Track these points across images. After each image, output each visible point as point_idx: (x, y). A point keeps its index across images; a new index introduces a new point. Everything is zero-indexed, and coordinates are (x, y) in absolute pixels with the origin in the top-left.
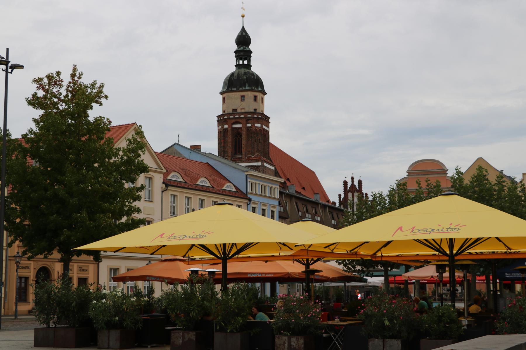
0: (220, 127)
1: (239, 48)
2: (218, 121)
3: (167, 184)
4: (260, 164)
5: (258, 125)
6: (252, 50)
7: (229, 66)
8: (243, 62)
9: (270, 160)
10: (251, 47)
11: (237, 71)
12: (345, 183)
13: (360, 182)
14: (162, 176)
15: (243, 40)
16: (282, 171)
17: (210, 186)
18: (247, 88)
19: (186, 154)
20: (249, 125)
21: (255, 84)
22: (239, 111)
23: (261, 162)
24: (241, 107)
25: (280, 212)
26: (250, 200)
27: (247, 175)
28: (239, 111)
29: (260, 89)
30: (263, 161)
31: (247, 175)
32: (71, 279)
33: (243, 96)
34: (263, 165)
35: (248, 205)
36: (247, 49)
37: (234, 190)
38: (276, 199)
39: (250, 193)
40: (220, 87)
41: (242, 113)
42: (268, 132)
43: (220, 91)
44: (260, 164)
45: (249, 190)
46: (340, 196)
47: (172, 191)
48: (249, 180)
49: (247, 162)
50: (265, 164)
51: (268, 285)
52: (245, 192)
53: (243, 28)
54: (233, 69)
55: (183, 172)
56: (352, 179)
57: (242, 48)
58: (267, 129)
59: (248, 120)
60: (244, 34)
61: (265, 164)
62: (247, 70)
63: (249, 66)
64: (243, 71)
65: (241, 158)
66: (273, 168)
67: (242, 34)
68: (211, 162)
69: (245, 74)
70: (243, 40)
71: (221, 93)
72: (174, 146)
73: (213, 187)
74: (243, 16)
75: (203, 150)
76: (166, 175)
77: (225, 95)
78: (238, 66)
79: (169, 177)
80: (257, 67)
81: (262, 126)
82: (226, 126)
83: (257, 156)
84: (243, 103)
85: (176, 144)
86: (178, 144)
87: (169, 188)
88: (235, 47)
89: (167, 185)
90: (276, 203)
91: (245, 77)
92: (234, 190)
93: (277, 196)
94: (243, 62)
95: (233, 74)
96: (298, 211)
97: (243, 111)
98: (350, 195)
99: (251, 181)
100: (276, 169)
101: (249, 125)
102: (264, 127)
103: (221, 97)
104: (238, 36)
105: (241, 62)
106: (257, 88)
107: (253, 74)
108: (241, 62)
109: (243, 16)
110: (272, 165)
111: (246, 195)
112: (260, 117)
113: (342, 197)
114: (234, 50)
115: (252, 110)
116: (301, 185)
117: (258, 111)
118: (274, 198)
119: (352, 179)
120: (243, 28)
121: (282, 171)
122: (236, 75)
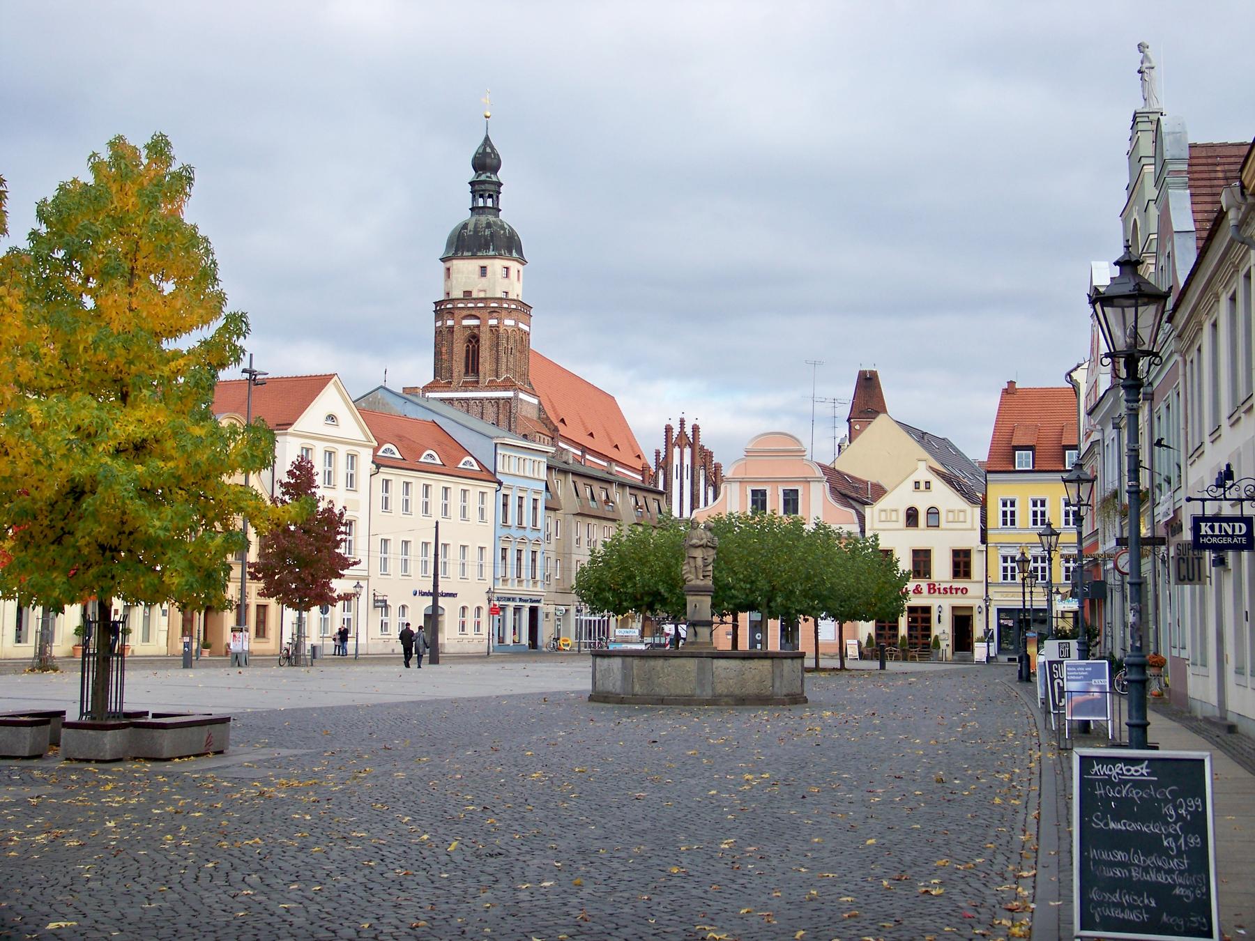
3: (379, 464)
4: (510, 394)
5: (509, 322)
7: (458, 208)
8: (485, 202)
11: (474, 219)
12: (668, 429)
13: (695, 429)
14: (371, 451)
15: (486, 162)
16: (553, 407)
18: (492, 253)
19: (399, 407)
21: (509, 245)
22: (474, 295)
24: (480, 287)
25: (546, 500)
26: (500, 484)
28: (474, 295)
29: (514, 254)
32: (247, 606)
33: (483, 270)
34: (516, 397)
36: (494, 179)
41: (481, 300)
43: (441, 256)
44: (510, 394)
45: (499, 468)
46: (658, 453)
47: (385, 473)
48: (499, 451)
51: (744, 645)
53: (487, 139)
55: (399, 440)
56: (682, 422)
58: (526, 328)
61: (522, 396)
62: (492, 218)
65: (477, 382)
66: (535, 401)
68: (439, 420)
69: (489, 225)
70: (486, 162)
71: (443, 260)
76: (376, 450)
77: (448, 264)
79: (380, 453)
80: (513, 210)
81: (516, 324)
83: (507, 379)
84: (483, 279)
87: (382, 469)
88: (471, 174)
89: (378, 467)
91: (487, 232)
92: (476, 467)
94: (485, 202)
97: (482, 295)
98: (676, 451)
100: (540, 403)
102: (521, 325)
105: (481, 203)
106: (511, 253)
108: (481, 203)
110: (535, 395)
113: (662, 455)
115: (500, 295)
116: (586, 429)
117: (510, 297)
119: (682, 422)
120: (487, 139)
121: (553, 407)
122: (471, 227)
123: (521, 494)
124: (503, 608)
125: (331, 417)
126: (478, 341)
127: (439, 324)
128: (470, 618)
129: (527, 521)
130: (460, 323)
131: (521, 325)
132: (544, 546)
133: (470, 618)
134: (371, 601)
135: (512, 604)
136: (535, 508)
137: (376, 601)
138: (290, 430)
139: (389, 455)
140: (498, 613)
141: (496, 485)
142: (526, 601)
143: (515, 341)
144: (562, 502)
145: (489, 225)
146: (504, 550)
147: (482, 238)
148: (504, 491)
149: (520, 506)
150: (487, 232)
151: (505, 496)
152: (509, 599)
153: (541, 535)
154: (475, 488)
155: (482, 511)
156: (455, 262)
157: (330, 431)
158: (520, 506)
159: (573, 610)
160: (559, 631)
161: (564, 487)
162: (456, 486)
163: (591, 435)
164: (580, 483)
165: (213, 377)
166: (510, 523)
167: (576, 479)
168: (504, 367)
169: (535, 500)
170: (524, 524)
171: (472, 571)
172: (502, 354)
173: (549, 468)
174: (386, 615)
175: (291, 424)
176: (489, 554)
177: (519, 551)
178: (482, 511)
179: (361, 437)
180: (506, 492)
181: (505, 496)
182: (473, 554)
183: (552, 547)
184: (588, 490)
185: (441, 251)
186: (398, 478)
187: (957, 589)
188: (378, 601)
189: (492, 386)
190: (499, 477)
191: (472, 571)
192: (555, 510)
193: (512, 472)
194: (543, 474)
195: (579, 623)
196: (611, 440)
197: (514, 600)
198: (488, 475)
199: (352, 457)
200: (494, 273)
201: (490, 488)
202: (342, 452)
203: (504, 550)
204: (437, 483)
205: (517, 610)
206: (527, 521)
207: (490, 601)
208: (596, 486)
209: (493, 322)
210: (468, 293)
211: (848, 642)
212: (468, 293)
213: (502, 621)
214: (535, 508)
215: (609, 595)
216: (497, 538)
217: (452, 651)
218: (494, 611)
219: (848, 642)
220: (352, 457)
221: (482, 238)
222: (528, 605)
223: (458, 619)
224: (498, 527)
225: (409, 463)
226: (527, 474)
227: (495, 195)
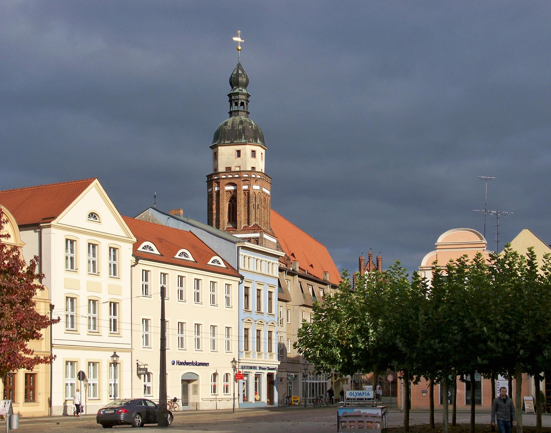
3: (138, 256)
4: (258, 235)
5: (256, 187)
14: (131, 246)
18: (243, 141)
22: (233, 170)
24: (236, 164)
26: (242, 278)
28: (233, 170)
33: (239, 152)
34: (262, 237)
44: (258, 235)
45: (241, 266)
47: (144, 265)
55: (158, 242)
66: (275, 241)
76: (135, 246)
77: (215, 150)
79: (140, 249)
81: (261, 189)
84: (239, 159)
87: (140, 261)
91: (240, 127)
92: (223, 265)
97: (238, 169)
100: (278, 242)
102: (264, 190)
106: (256, 141)
120: (239, 65)
122: (229, 124)
123: (259, 288)
124: (246, 375)
125: (93, 215)
126: (236, 200)
127: (210, 190)
128: (220, 383)
129: (264, 307)
130: (223, 189)
131: (264, 190)
132: (279, 328)
133: (220, 383)
134: (135, 373)
135: (254, 372)
136: (270, 299)
137: (139, 369)
138: (53, 223)
140: (242, 378)
141: (239, 279)
142: (264, 369)
143: (261, 200)
144: (292, 298)
145: (241, 122)
146: (246, 330)
148: (245, 284)
149: (259, 297)
150: (240, 127)
151: (247, 288)
152: (251, 368)
153: (275, 319)
154: (222, 281)
155: (228, 299)
156: (220, 148)
157: (92, 226)
158: (259, 297)
159: (300, 376)
160: (290, 391)
161: (293, 285)
162: (206, 278)
163: (312, 266)
164: (304, 282)
166: (251, 308)
167: (301, 280)
168: (253, 218)
169: (270, 293)
170: (262, 311)
171: (221, 345)
172: (252, 209)
173: (281, 270)
174: (149, 381)
175: (54, 218)
176: (234, 332)
177: (258, 331)
178: (228, 299)
179: (122, 234)
180: (247, 285)
181: (247, 288)
182: (221, 331)
183: (284, 329)
184: (310, 289)
186: (156, 270)
188: (141, 369)
189: (246, 230)
190: (241, 272)
191: (221, 345)
192: (286, 301)
193: (251, 269)
194: (276, 273)
195: (305, 385)
196: (323, 269)
197: (255, 368)
198: (232, 271)
199: (114, 250)
200: (245, 155)
201: (234, 281)
202: (104, 246)
203: (246, 330)
204: (190, 275)
205: (257, 376)
206: (264, 307)
207: (234, 368)
208: (316, 286)
209: (245, 187)
210: (228, 169)
211: (526, 398)
212: (228, 169)
213: (247, 384)
214: (270, 299)
215: (337, 352)
216: (240, 320)
217: (206, 408)
218: (238, 377)
219: (526, 398)
220: (114, 250)
222: (266, 372)
223: (211, 383)
224: (242, 312)
225: (166, 257)
226: (263, 272)
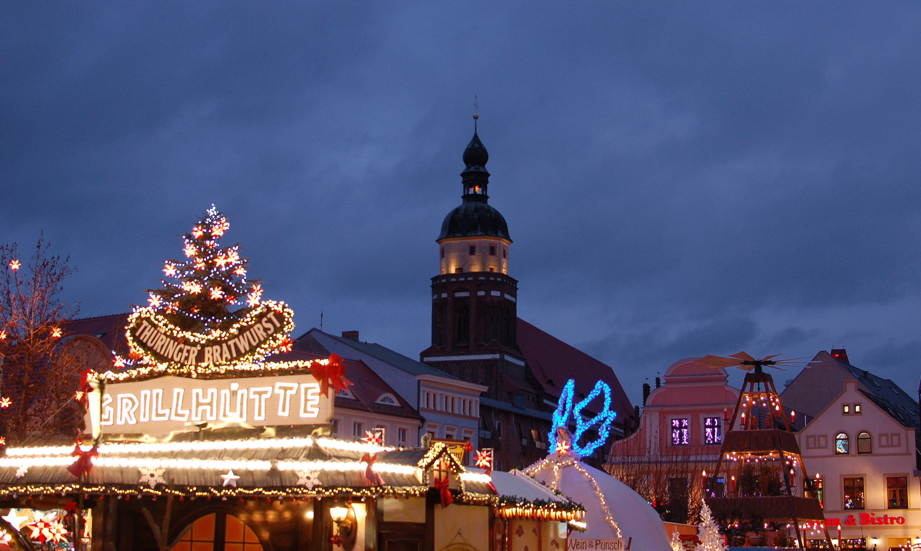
0: (435, 297)
1: (468, 168)
2: (432, 286)
4: (497, 356)
6: (489, 172)
9: (518, 349)
10: (489, 167)
15: (476, 156)
17: (353, 398)
20: (481, 293)
21: (495, 225)
23: (499, 353)
26: (423, 420)
27: (419, 381)
30: (502, 353)
31: (419, 381)
34: (502, 358)
35: (419, 428)
36: (482, 170)
37: (396, 403)
38: (475, 419)
39: (424, 409)
40: (437, 231)
42: (515, 304)
44: (497, 356)
45: (423, 405)
48: (422, 389)
49: (476, 354)
50: (507, 358)
52: (415, 408)
53: (476, 136)
54: (459, 202)
57: (472, 169)
58: (514, 300)
59: (480, 286)
60: (477, 145)
61: (507, 358)
62: (480, 204)
63: (484, 198)
64: (473, 205)
66: (522, 364)
67: (473, 145)
68: (368, 360)
69: (477, 210)
70: (476, 156)
72: (312, 333)
73: (358, 400)
74: (476, 118)
75: (362, 339)
78: (466, 197)
81: (502, 295)
82: (444, 295)
85: (314, 329)
86: (320, 332)
88: (463, 167)
90: (475, 425)
91: (476, 216)
92: (396, 403)
93: (476, 413)
95: (457, 211)
96: (521, 437)
99: (427, 390)
100: (526, 364)
101: (481, 293)
102: (507, 296)
103: (438, 246)
104: (467, 149)
107: (490, 210)
109: (476, 118)
111: (418, 412)
112: (499, 279)
114: (462, 172)
118: (470, 417)
120: (476, 136)
131: (507, 296)
139: (387, 403)
147: (475, 220)
165: (7, 268)
185: (438, 233)
187: (892, 519)
190: (422, 414)
221: (475, 220)
227: (484, 184)
